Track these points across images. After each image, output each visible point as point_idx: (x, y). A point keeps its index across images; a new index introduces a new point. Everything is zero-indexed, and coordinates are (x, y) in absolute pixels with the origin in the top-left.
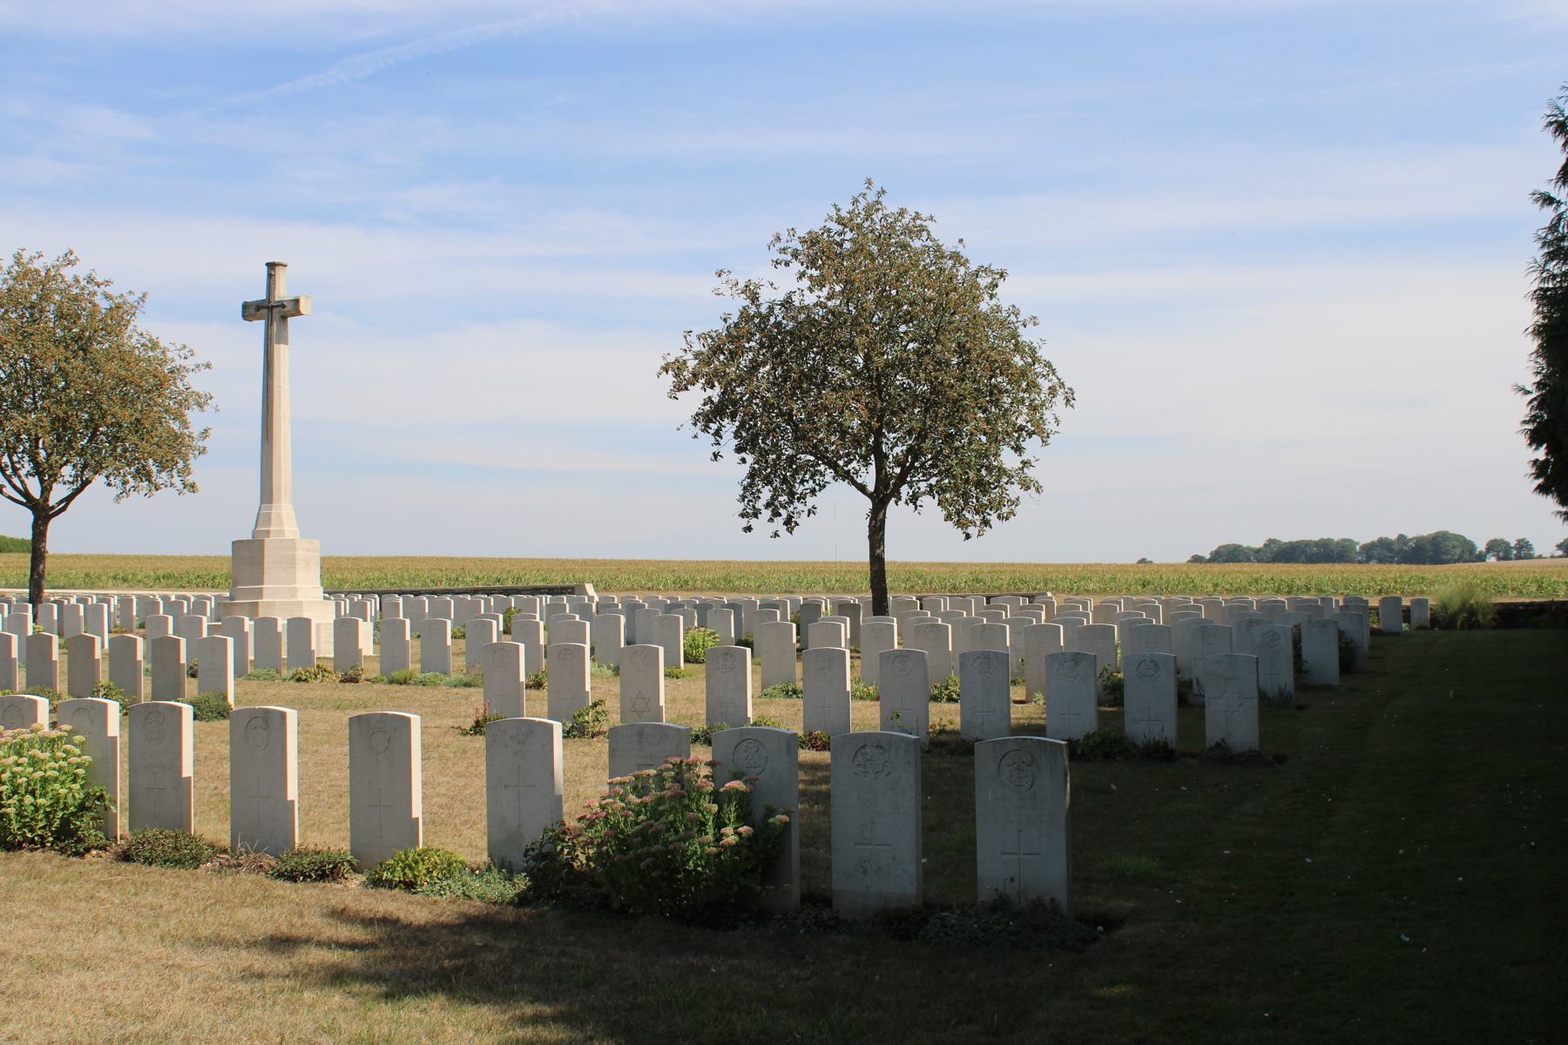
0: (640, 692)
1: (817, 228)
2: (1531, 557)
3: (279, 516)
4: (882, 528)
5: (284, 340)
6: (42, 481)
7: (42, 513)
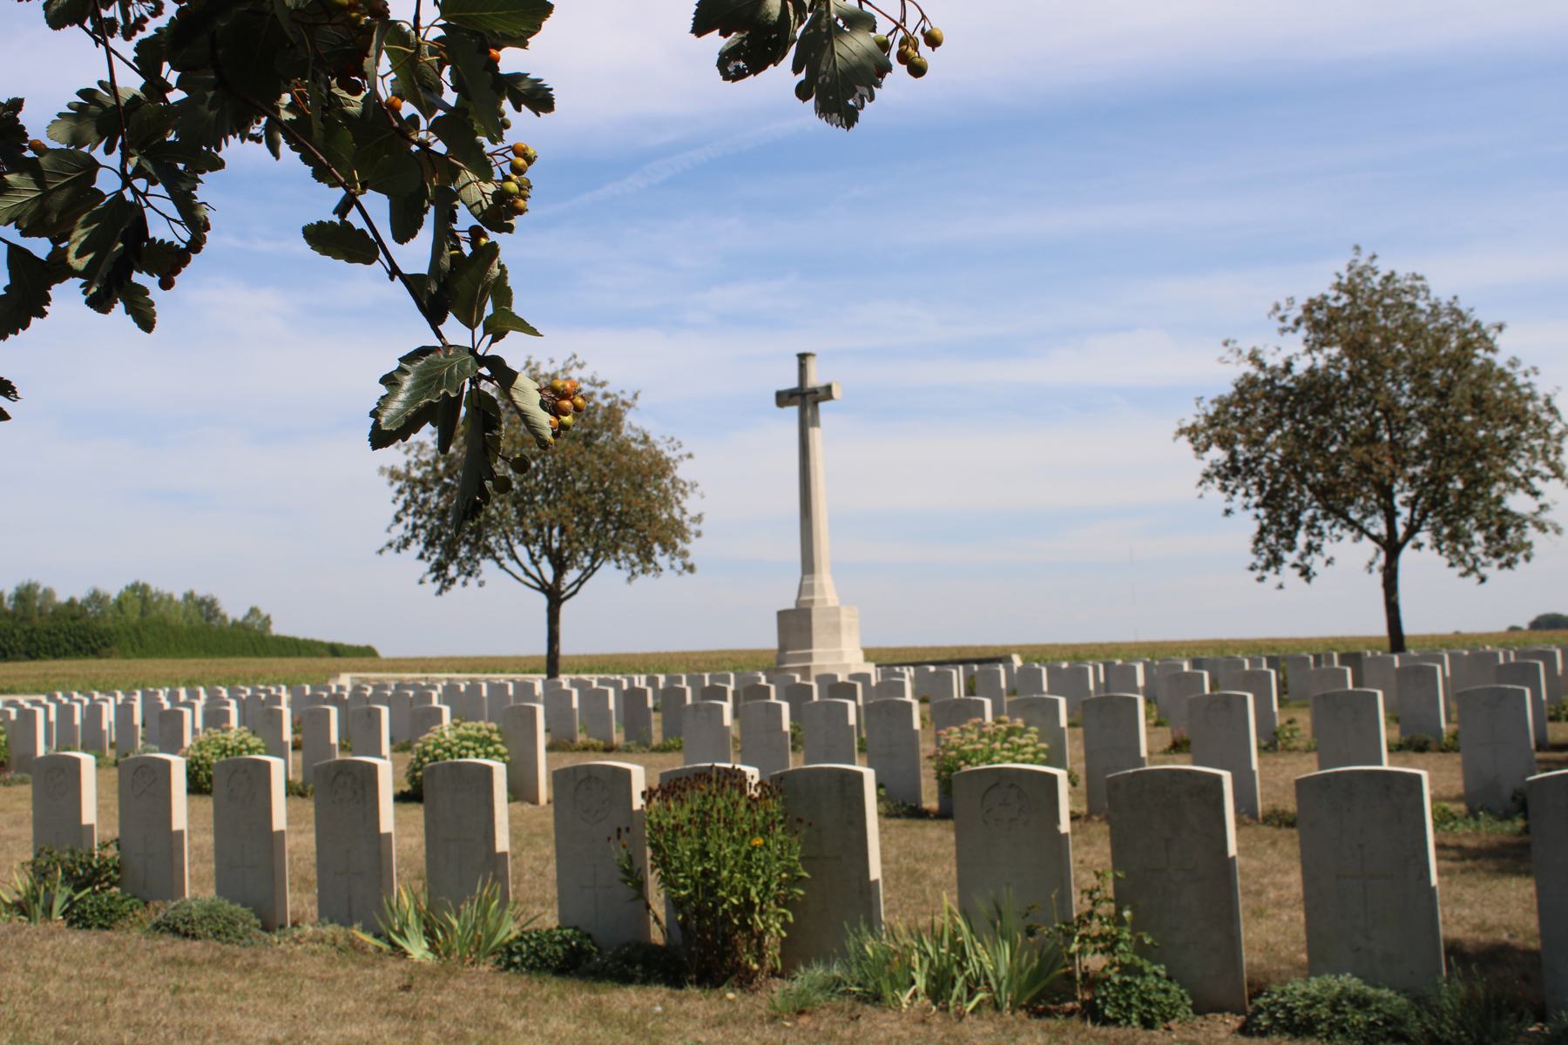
1: (1315, 295)
3: (821, 586)
5: (816, 423)
7: (555, 597)
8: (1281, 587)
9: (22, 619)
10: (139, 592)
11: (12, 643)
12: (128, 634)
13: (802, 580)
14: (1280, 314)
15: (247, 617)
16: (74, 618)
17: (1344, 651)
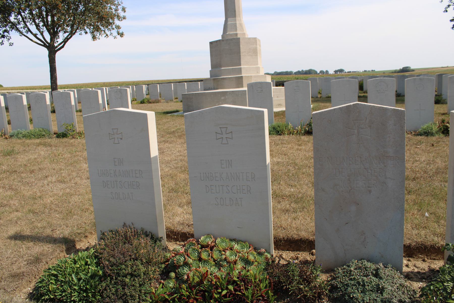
2: (328, 74)
3: (241, 25)
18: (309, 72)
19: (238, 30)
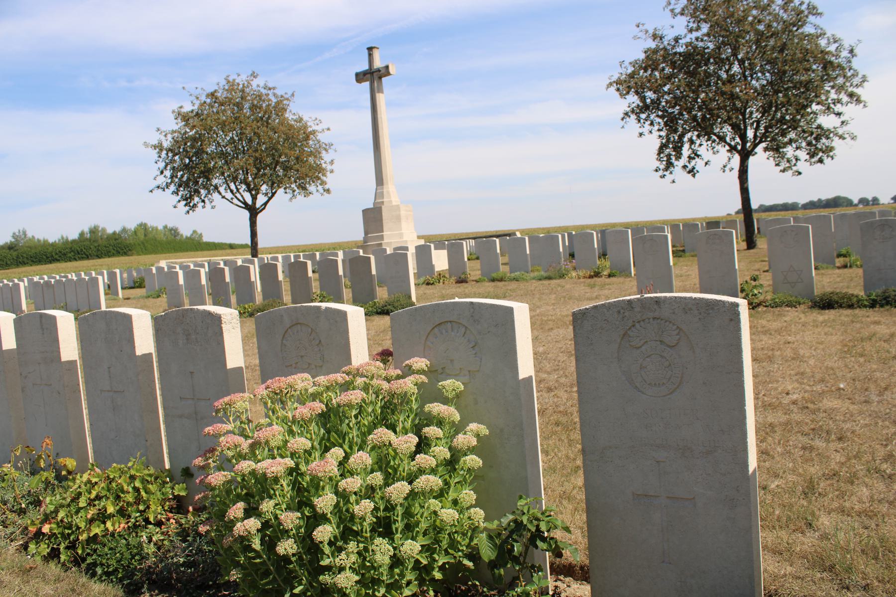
0: (791, 266)
2: (878, 204)
3: (388, 192)
4: (746, 171)
5: (381, 90)
6: (252, 195)
7: (254, 212)
8: (674, 182)
9: (94, 241)
10: (143, 226)
11: (90, 252)
12: (139, 245)
13: (376, 189)
14: (671, 7)
15: (192, 235)
16: (116, 240)
17: (707, 221)
18: (835, 203)
19: (385, 197)
